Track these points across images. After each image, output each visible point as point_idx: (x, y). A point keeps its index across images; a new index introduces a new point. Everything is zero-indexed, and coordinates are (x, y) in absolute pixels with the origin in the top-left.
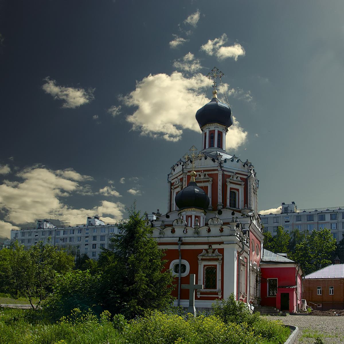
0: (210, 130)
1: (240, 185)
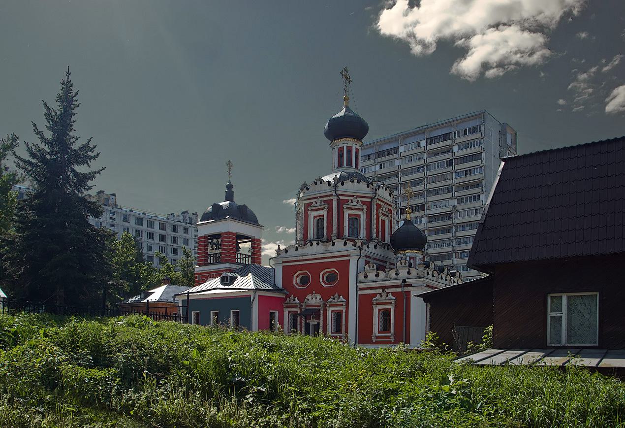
0: (348, 145)
1: (362, 210)
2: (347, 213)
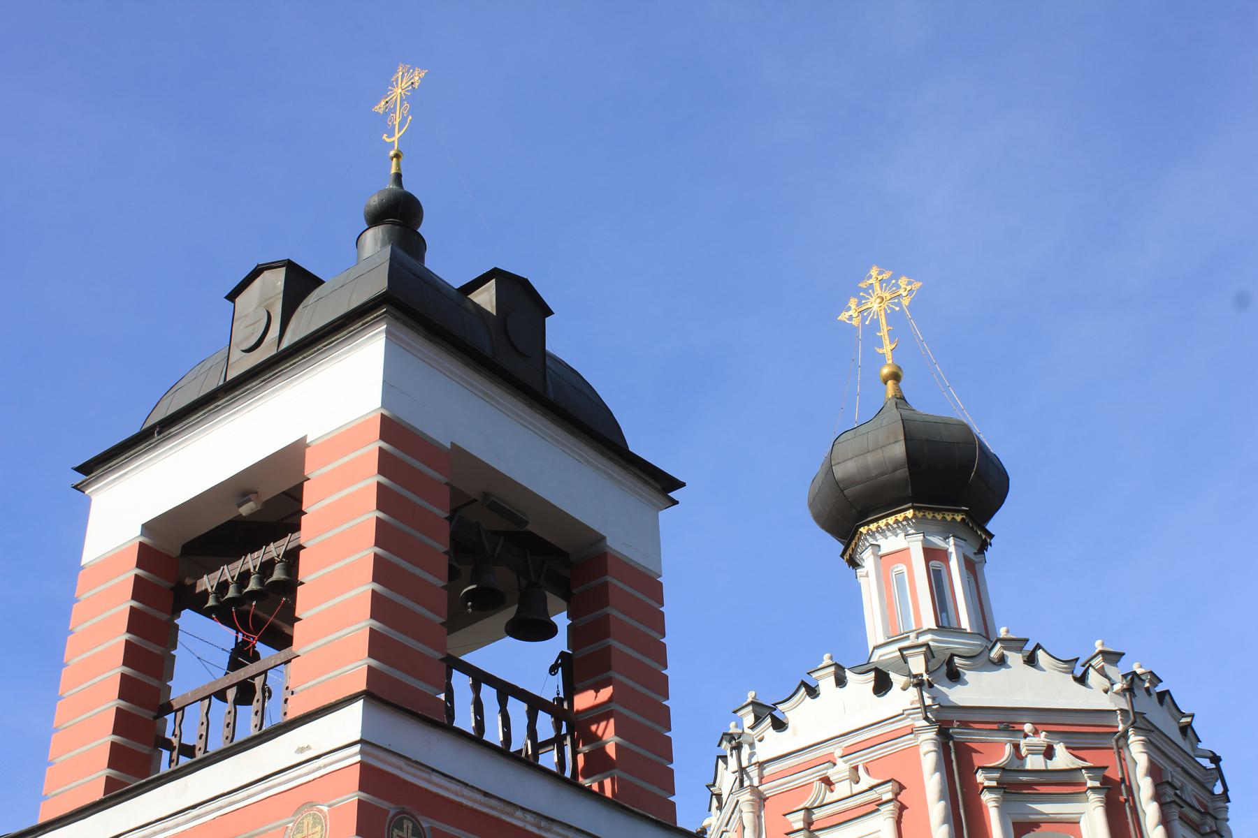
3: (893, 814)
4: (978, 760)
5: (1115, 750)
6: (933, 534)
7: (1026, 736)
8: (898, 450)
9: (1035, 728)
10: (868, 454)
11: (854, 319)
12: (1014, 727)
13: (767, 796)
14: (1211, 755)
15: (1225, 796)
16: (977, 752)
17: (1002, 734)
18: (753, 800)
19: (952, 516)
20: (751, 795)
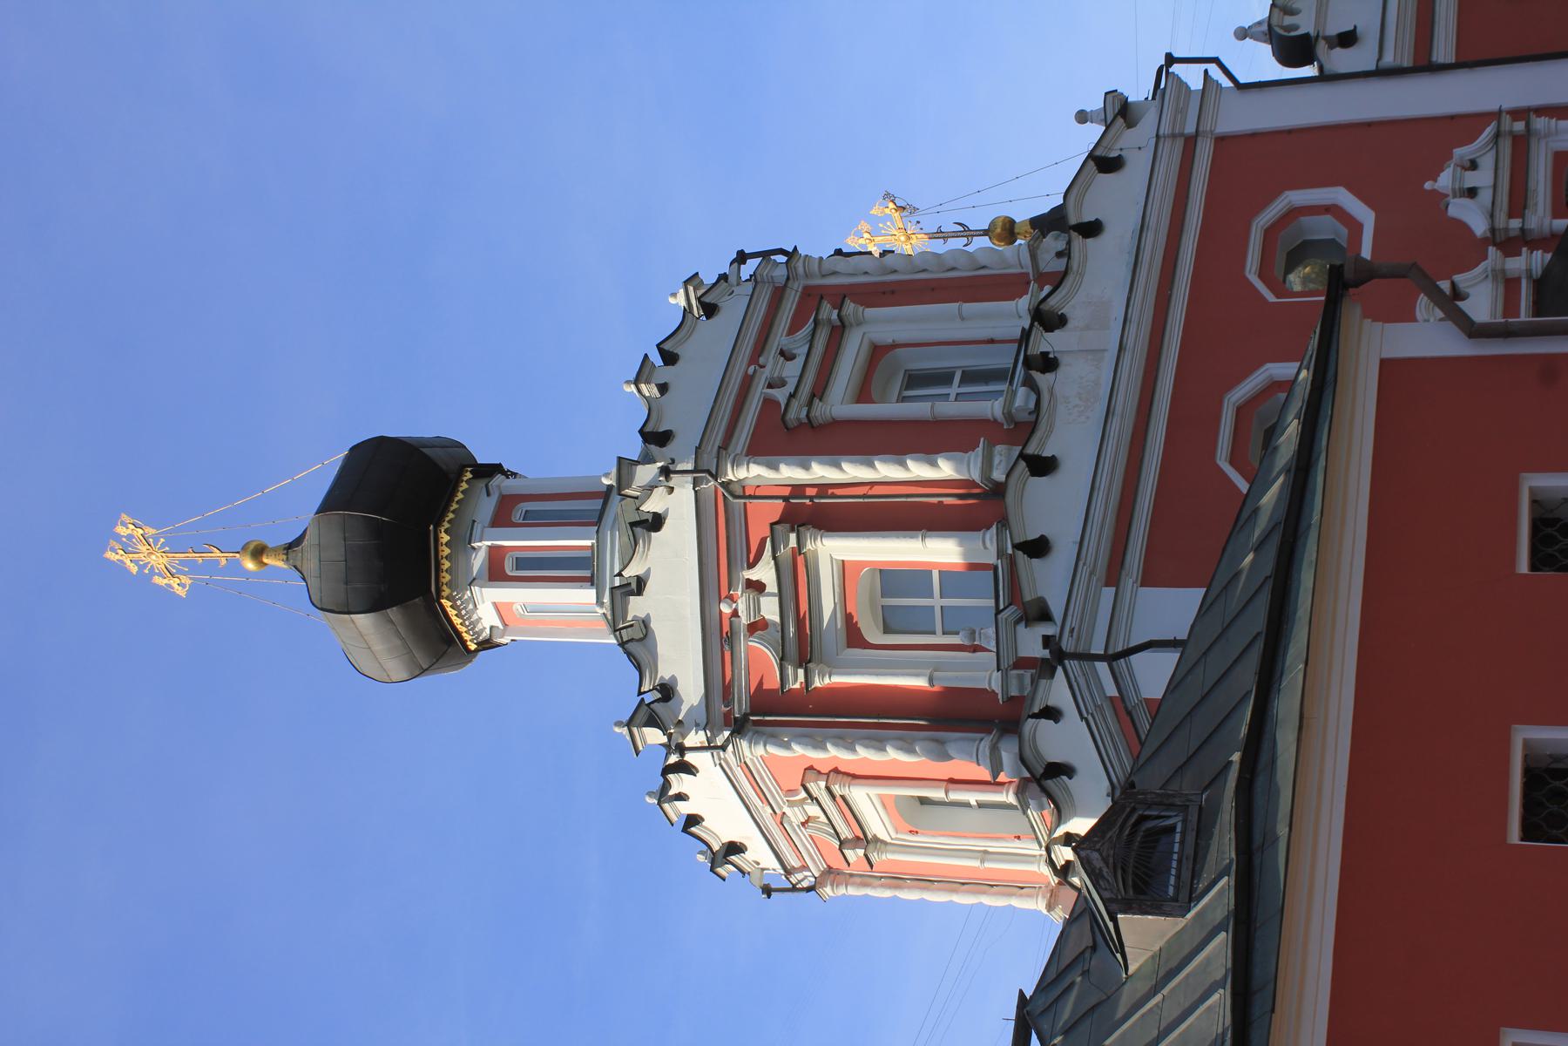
2: (839, 404)
3: (844, 786)
4: (773, 682)
5: (747, 501)
6: (469, 567)
7: (735, 614)
8: (363, 621)
9: (726, 597)
10: (373, 649)
11: (183, 582)
12: (727, 633)
13: (825, 866)
14: (736, 265)
15: (791, 255)
16: (761, 683)
17: (736, 649)
18: (832, 885)
19: (445, 573)
20: (826, 887)
